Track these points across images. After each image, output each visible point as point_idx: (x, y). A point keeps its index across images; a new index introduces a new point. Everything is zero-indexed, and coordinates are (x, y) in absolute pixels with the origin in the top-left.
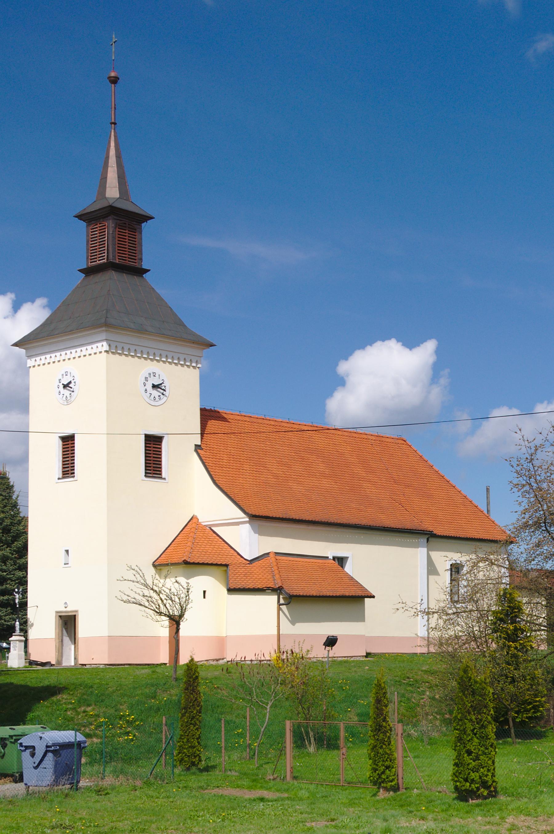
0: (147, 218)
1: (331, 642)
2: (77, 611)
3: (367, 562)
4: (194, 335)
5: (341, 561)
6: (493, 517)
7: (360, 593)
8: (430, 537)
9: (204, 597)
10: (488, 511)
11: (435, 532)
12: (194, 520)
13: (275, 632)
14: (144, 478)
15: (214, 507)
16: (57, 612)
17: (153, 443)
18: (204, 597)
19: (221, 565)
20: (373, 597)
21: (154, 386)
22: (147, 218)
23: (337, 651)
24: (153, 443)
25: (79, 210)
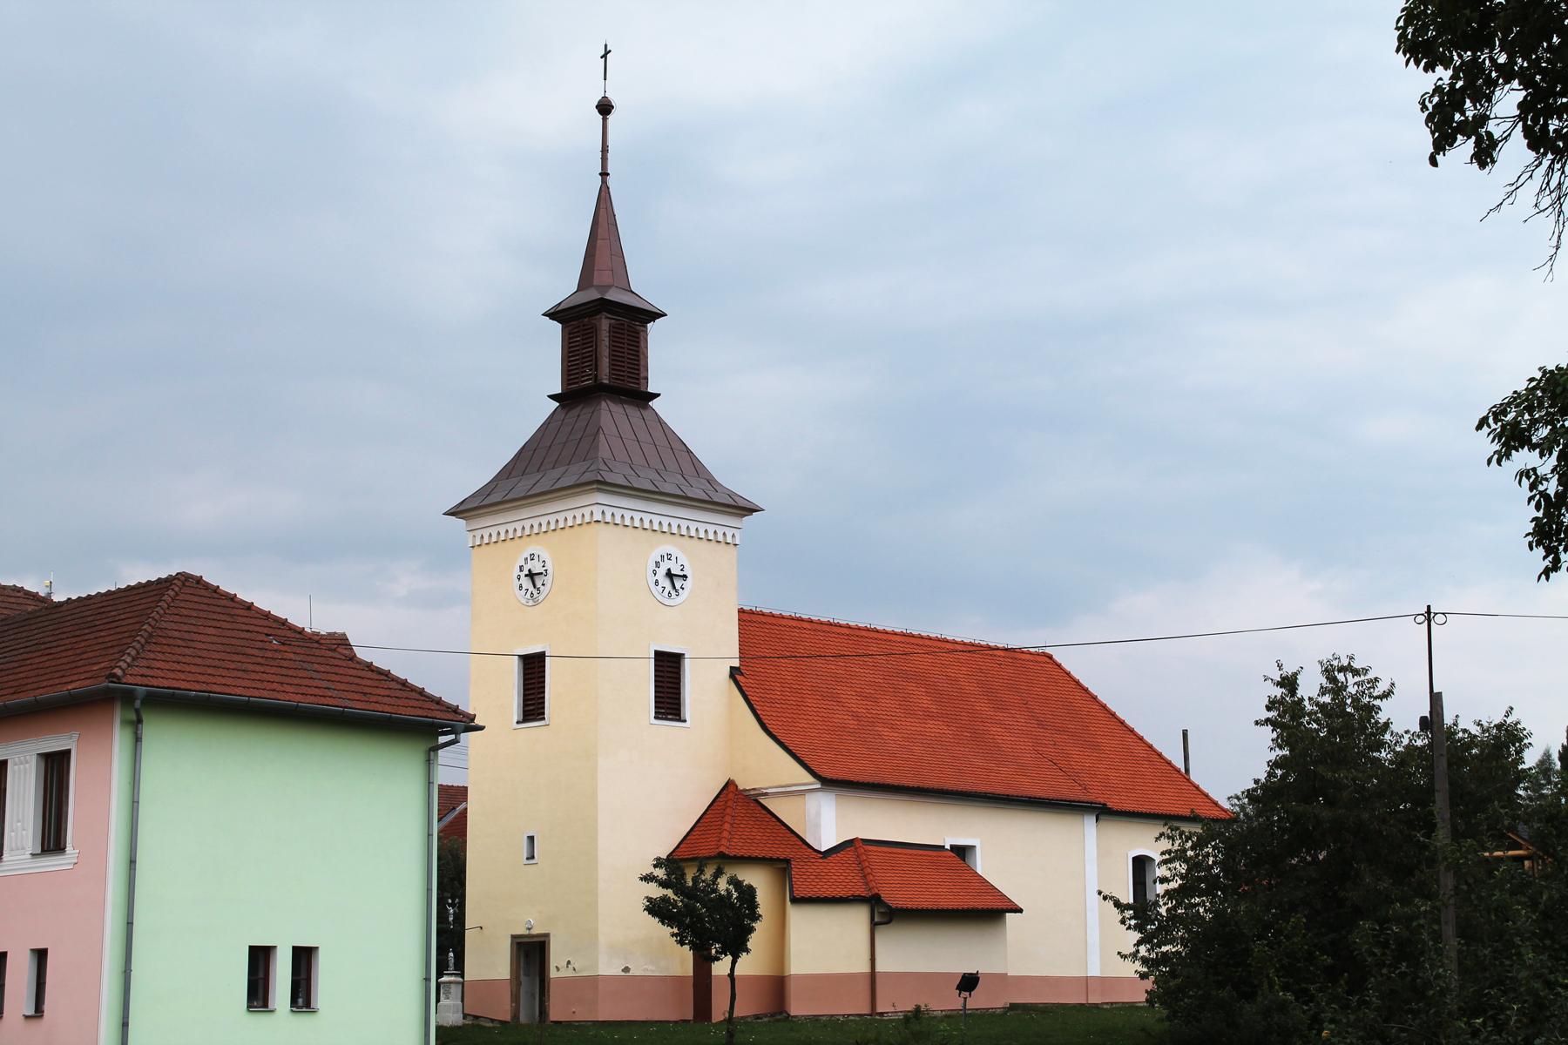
0: (656, 315)
1: (969, 982)
2: (547, 935)
3: (1005, 848)
4: (731, 494)
5: (962, 852)
6: (1193, 777)
7: (999, 905)
8: (1103, 812)
9: (1185, 733)
10: (1187, 770)
11: (1110, 805)
12: (731, 788)
13: (866, 969)
14: (654, 721)
15: (768, 767)
16: (513, 937)
17: (668, 668)
18: (1185, 733)
19: (778, 860)
20: (1021, 911)
21: (670, 575)
22: (656, 315)
23: (978, 1000)
24: (668, 668)
25: (549, 305)
